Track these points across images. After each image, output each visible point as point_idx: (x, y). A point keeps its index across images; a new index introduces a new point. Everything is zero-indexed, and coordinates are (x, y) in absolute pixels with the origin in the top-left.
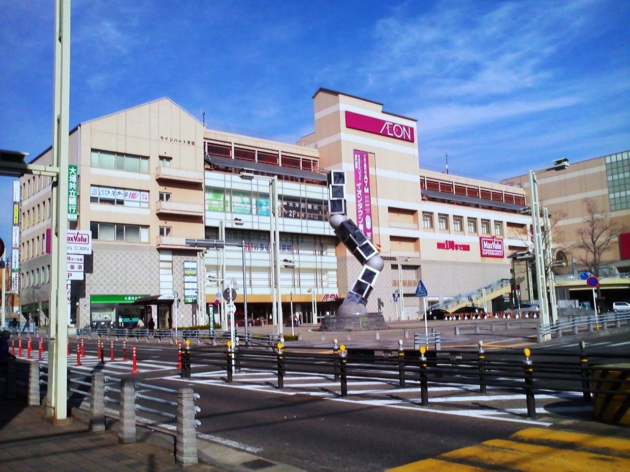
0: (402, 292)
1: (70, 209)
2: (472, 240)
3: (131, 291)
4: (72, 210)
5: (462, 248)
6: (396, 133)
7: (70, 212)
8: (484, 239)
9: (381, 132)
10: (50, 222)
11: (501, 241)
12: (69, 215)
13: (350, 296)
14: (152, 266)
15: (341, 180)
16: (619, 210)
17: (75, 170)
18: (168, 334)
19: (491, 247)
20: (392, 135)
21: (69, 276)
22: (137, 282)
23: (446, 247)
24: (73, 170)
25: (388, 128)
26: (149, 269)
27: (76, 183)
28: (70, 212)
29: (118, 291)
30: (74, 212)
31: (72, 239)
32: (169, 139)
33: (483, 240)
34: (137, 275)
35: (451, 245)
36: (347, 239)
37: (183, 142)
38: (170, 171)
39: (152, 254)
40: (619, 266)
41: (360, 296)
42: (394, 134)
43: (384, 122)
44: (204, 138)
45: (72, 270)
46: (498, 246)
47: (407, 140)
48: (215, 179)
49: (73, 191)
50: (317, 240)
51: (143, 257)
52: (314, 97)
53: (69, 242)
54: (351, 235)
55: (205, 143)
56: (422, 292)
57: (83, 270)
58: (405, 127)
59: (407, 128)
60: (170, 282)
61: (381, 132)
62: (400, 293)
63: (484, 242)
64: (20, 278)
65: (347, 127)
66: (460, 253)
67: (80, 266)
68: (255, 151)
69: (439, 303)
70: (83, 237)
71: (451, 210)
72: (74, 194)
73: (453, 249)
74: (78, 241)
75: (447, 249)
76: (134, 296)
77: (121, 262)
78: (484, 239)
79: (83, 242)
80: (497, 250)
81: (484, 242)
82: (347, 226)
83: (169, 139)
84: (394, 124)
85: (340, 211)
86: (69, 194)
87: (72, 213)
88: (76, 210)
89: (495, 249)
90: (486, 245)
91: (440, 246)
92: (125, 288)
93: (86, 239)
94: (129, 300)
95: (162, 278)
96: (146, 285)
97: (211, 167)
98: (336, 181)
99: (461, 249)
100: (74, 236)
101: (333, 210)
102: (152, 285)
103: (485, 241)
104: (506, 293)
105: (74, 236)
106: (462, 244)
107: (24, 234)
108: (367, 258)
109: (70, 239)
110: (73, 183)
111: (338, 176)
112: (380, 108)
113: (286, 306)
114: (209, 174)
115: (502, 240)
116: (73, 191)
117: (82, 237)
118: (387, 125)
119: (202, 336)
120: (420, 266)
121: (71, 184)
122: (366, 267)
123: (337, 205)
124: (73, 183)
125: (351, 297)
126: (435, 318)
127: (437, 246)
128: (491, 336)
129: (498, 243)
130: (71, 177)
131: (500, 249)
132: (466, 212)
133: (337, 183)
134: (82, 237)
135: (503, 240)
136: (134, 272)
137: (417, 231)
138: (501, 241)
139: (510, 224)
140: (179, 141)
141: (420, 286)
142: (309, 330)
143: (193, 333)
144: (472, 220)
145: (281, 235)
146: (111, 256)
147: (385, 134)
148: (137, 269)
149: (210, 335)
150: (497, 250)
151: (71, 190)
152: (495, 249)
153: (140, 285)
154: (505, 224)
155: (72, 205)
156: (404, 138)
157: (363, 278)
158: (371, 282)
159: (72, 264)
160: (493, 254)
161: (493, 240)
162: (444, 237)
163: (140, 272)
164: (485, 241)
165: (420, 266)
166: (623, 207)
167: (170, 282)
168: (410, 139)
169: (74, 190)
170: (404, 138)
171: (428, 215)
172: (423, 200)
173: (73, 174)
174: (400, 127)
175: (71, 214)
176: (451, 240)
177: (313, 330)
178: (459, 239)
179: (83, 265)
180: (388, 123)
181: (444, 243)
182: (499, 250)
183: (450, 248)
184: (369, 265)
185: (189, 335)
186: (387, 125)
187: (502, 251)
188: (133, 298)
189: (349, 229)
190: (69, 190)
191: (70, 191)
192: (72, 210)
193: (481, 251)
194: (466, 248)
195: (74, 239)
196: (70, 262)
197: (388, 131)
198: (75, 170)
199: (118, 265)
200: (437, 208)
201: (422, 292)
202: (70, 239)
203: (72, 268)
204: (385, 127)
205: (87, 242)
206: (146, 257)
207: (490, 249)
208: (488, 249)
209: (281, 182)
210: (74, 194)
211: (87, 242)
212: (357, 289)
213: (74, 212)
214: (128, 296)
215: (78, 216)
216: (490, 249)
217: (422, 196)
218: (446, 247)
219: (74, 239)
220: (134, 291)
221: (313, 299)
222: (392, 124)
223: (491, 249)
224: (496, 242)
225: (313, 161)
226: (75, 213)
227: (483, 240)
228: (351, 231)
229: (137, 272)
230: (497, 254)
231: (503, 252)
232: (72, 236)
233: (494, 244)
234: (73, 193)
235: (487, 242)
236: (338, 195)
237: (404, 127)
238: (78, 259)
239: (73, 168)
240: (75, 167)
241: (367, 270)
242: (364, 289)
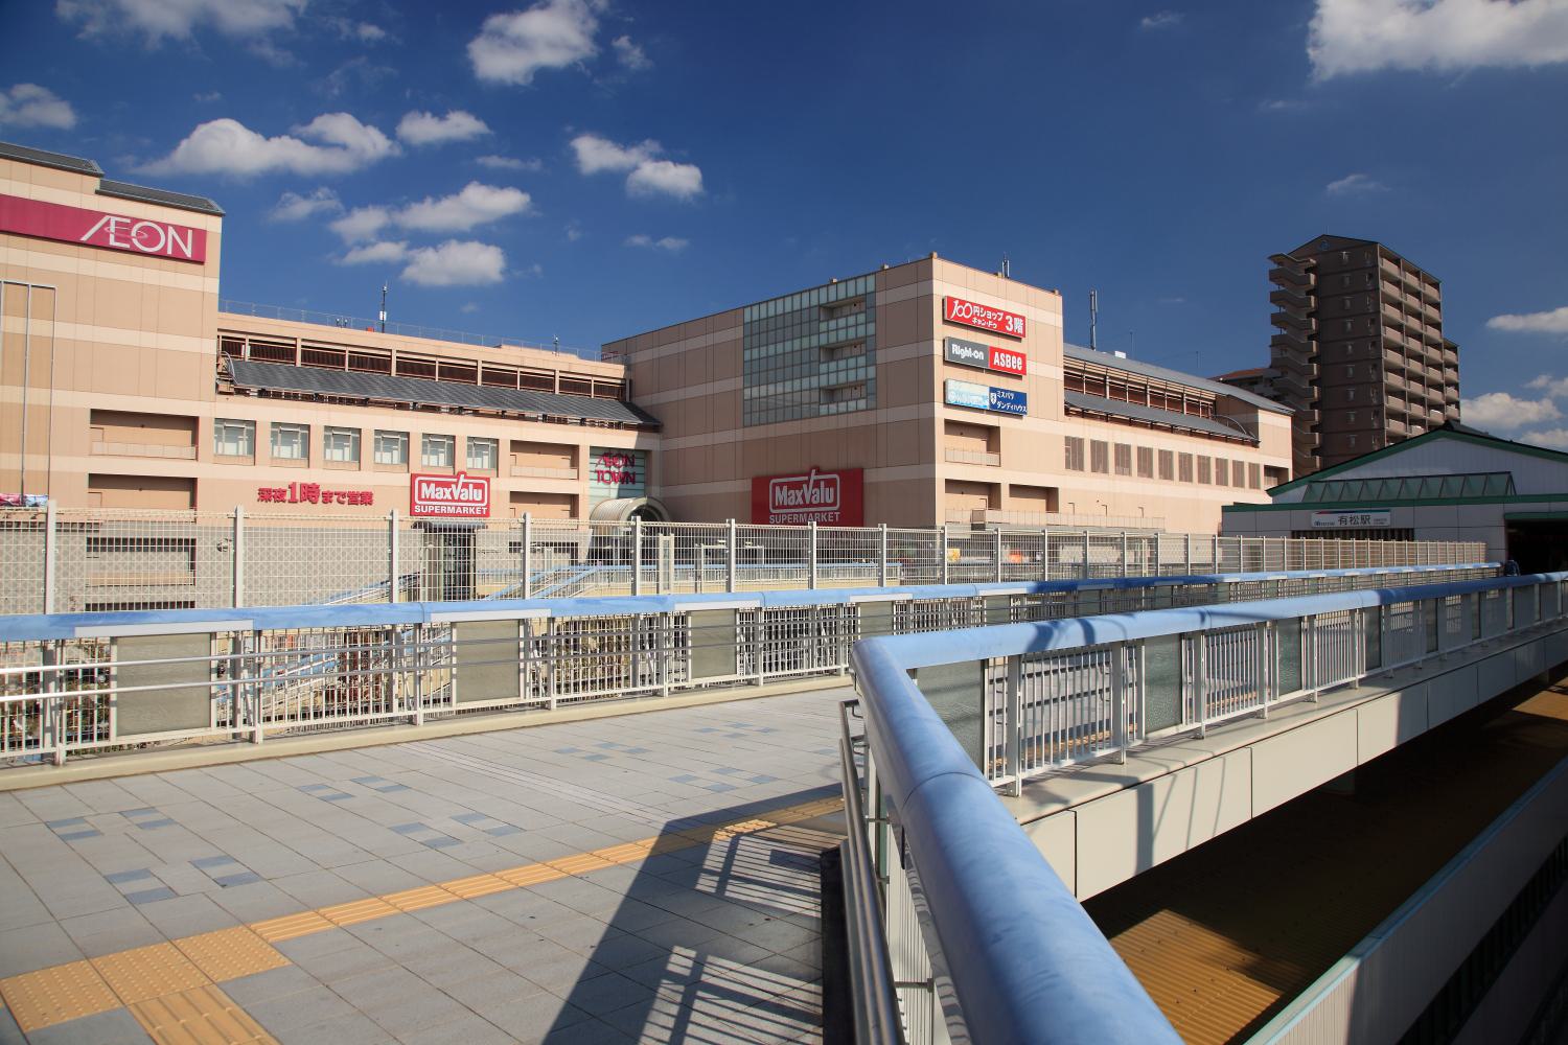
6: (140, 241)
8: (422, 478)
10: (1377, 649)
16: (797, 420)
19: (801, 501)
20: (127, 246)
33: (420, 482)
42: (132, 245)
47: (178, 257)
60: (697, 1011)
63: (777, 488)
66: (339, 511)
78: (422, 478)
80: (791, 507)
89: (811, 505)
103: (781, 485)
106: (347, 490)
112: (95, 183)
113: (76, 739)
115: (488, 480)
118: (108, 224)
139: (518, 446)
145: (1225, 513)
147: (99, 244)
152: (459, 500)
154: (505, 448)
164: (428, 483)
166: (806, 414)
167: (697, 1011)
181: (286, 488)
186: (108, 224)
193: (412, 504)
200: (268, 412)
204: (101, 229)
207: (795, 507)
208: (788, 507)
216: (795, 507)
223: (447, 500)
227: (775, 485)
231: (488, 506)
233: (807, 491)
235: (433, 485)
237: (171, 229)
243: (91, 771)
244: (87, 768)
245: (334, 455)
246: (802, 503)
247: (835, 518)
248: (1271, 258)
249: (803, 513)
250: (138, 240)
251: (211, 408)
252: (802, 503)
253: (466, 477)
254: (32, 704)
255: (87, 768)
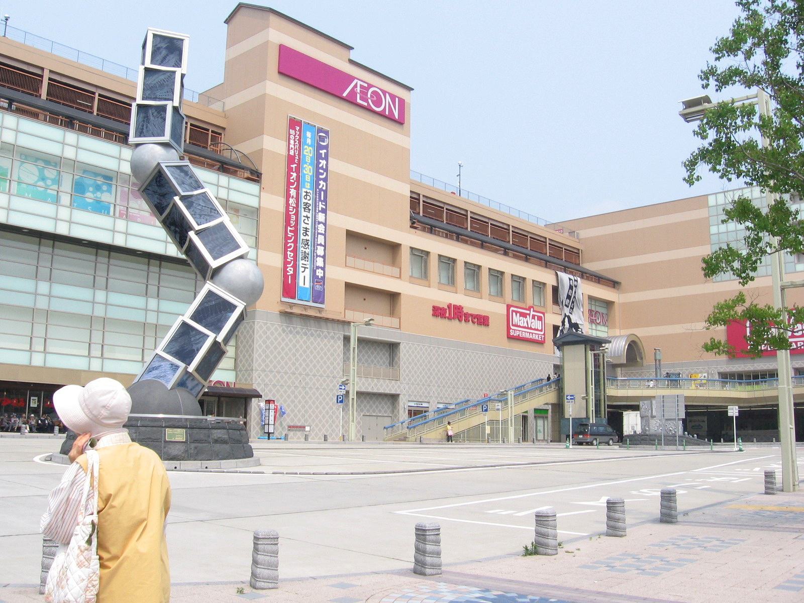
0: (353, 389)
2: (494, 308)
5: (476, 320)
9: (345, 95)
11: (542, 315)
15: (172, 58)
20: (365, 104)
23: (447, 315)
25: (359, 91)
35: (457, 313)
41: (182, 365)
42: (368, 103)
43: (351, 78)
46: (537, 324)
47: (390, 118)
53: (413, 418)
59: (393, 97)
61: (345, 95)
63: (514, 314)
66: (471, 328)
68: (94, 93)
69: (427, 414)
71: (463, 253)
73: (460, 321)
75: (450, 318)
80: (535, 329)
81: (514, 314)
84: (370, 86)
89: (531, 328)
90: (516, 319)
91: (438, 312)
98: (159, 58)
99: (473, 322)
101: (140, 133)
103: (516, 312)
104: (547, 404)
108: (214, 264)
111: (164, 45)
118: (356, 86)
122: (209, 286)
123: (152, 118)
127: (431, 312)
128: (93, 72)
129: (536, 317)
131: (540, 328)
132: (488, 260)
135: (546, 315)
137: (398, 281)
142: (37, 459)
147: (350, 101)
156: (387, 113)
157: (194, 317)
160: (527, 336)
161: (528, 312)
162: (445, 298)
168: (397, 117)
170: (387, 113)
171: (421, 256)
176: (458, 304)
178: (471, 304)
180: (359, 83)
181: (446, 307)
182: (537, 330)
186: (356, 86)
187: (542, 333)
193: (509, 329)
194: (482, 320)
197: (358, 96)
200: (437, 246)
204: (353, 89)
208: (519, 326)
211: (339, 397)
212: (176, 347)
218: (447, 315)
222: (366, 85)
224: (533, 317)
225: (212, 132)
227: (513, 311)
231: (544, 334)
233: (529, 319)
235: (518, 314)
236: (158, 94)
237: (387, 95)
241: (210, 294)
242: (195, 347)
243: (491, 498)
244: (594, 485)
246: (527, 326)
247: (542, 338)
248: (738, 178)
249: (527, 332)
250: (372, 101)
252: (527, 326)
255: (594, 485)
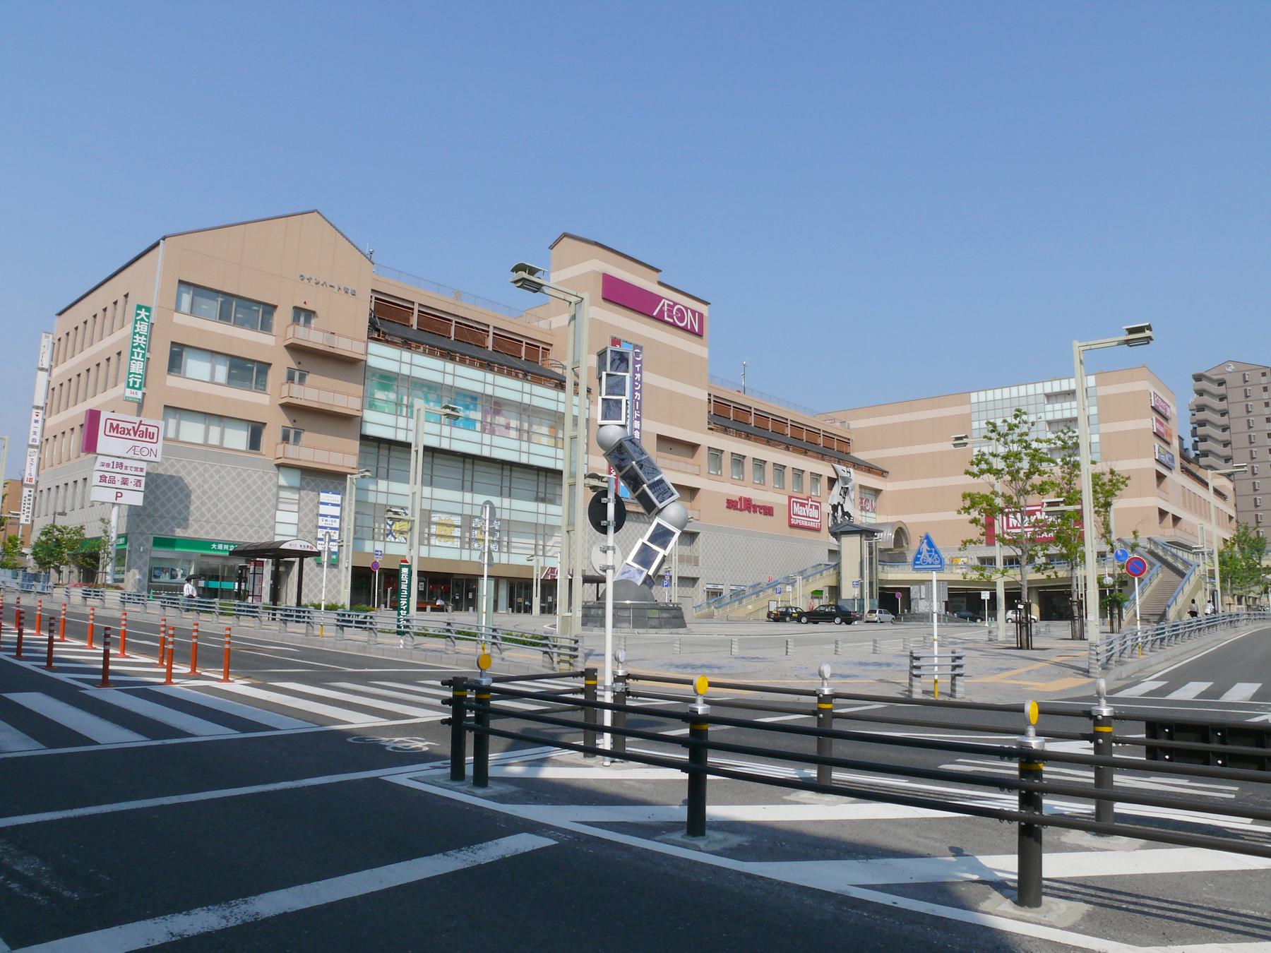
1: (131, 380)
3: (223, 534)
4: (135, 383)
5: (762, 511)
6: (677, 318)
7: (131, 385)
9: (655, 314)
12: (128, 390)
13: (627, 570)
14: (264, 494)
15: (624, 365)
17: (148, 314)
18: (304, 617)
20: (671, 321)
21: (117, 497)
22: (236, 519)
24: (143, 313)
25: (666, 310)
26: (259, 499)
27: (146, 336)
28: (131, 385)
29: (202, 532)
30: (137, 386)
31: (129, 433)
32: (313, 281)
34: (237, 507)
36: (627, 469)
37: (336, 288)
38: (313, 337)
39: (266, 473)
40: (981, 555)
41: (646, 571)
43: (660, 298)
44: (373, 290)
45: (123, 486)
46: (814, 513)
47: (692, 332)
48: (383, 357)
49: (139, 350)
50: (540, 477)
51: (250, 476)
52: (551, 248)
54: (634, 463)
55: (371, 297)
56: (930, 560)
57: (142, 488)
58: (691, 310)
59: (694, 312)
61: (655, 314)
62: (672, 573)
63: (795, 504)
64: (35, 498)
65: (603, 298)
66: (759, 517)
67: (139, 481)
70: (149, 431)
72: (141, 355)
73: (750, 512)
74: (139, 436)
75: (741, 510)
76: (229, 543)
77: (211, 482)
79: (148, 440)
80: (812, 518)
81: (795, 504)
82: (627, 445)
83: (313, 281)
84: (676, 304)
85: (618, 420)
86: (132, 354)
87: (133, 388)
88: (141, 383)
89: (809, 517)
90: (797, 508)
91: (731, 504)
92: (213, 528)
93: (153, 433)
94: (219, 550)
95: (280, 516)
96: (251, 526)
97: (379, 336)
98: (615, 366)
99: (760, 513)
100: (134, 427)
102: (261, 527)
103: (797, 502)
105: (134, 427)
107: (49, 422)
108: (660, 506)
109: (126, 432)
110: (141, 335)
114: (375, 348)
116: (139, 350)
117: (147, 429)
118: (663, 305)
119: (415, 630)
120: (699, 533)
121: (137, 337)
123: (612, 408)
124: (141, 335)
125: (627, 572)
126: (450, 608)
127: (726, 505)
130: (138, 326)
131: (817, 517)
133: (616, 370)
134: (147, 429)
136: (232, 501)
138: (818, 504)
140: (331, 286)
141: (925, 547)
143: (359, 619)
144: (780, 468)
146: (195, 468)
147: (659, 319)
148: (237, 496)
149: (399, 627)
150: (812, 518)
151: (136, 347)
153: (241, 525)
155: (135, 374)
156: (689, 327)
157: (649, 540)
158: (665, 548)
159: (125, 476)
160: (806, 524)
162: (737, 492)
163: (243, 503)
165: (699, 533)
168: (697, 331)
169: (142, 349)
170: (689, 327)
171: (716, 454)
172: (710, 429)
173: (142, 320)
174: (683, 308)
175: (133, 390)
176: (747, 497)
177: (550, 626)
179: (143, 480)
180: (667, 302)
181: (738, 500)
182: (815, 518)
183: (745, 510)
184: (663, 518)
185: (292, 616)
186: (663, 305)
187: (819, 521)
188: (226, 547)
189: (631, 452)
190: (133, 347)
191: (134, 350)
192: (135, 383)
193: (790, 517)
194: (768, 511)
195: (132, 432)
196: (121, 471)
197: (666, 313)
198: (148, 314)
199: (204, 509)
200: (730, 445)
201: (930, 560)
202: (126, 432)
203: (125, 484)
204: (661, 308)
205: (155, 440)
206: (255, 476)
209: (493, 375)
210: (141, 355)
213: (137, 386)
214: (217, 543)
215: (144, 394)
217: (709, 423)
219: (132, 432)
220: (229, 535)
221: (535, 573)
222: (672, 304)
226: (139, 389)
227: (794, 502)
228: (635, 456)
229: (242, 508)
230: (812, 525)
232: (130, 426)
234: (138, 353)
235: (798, 504)
236: (616, 390)
237: (689, 311)
238: (136, 469)
239: (143, 310)
240: (148, 309)
245: (558, 453)
251: (709, 439)
253: (812, 501)
254: (259, 387)
